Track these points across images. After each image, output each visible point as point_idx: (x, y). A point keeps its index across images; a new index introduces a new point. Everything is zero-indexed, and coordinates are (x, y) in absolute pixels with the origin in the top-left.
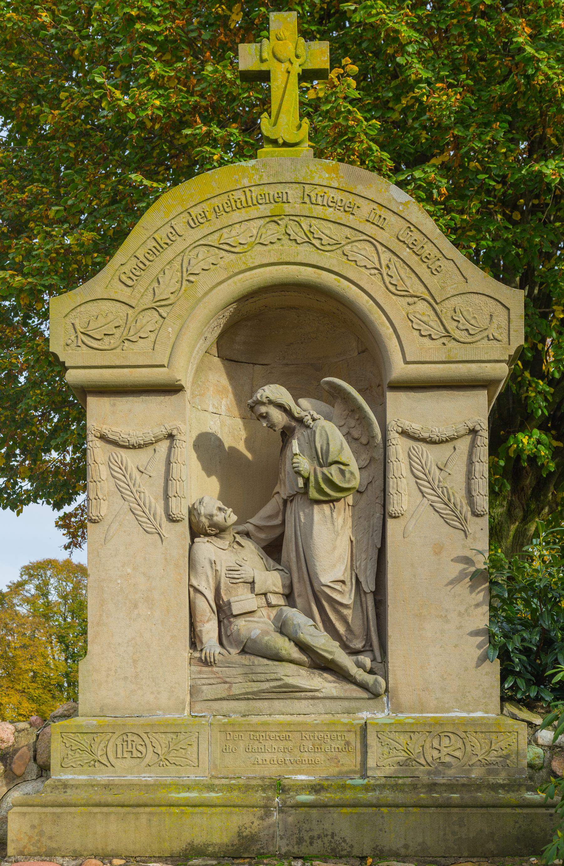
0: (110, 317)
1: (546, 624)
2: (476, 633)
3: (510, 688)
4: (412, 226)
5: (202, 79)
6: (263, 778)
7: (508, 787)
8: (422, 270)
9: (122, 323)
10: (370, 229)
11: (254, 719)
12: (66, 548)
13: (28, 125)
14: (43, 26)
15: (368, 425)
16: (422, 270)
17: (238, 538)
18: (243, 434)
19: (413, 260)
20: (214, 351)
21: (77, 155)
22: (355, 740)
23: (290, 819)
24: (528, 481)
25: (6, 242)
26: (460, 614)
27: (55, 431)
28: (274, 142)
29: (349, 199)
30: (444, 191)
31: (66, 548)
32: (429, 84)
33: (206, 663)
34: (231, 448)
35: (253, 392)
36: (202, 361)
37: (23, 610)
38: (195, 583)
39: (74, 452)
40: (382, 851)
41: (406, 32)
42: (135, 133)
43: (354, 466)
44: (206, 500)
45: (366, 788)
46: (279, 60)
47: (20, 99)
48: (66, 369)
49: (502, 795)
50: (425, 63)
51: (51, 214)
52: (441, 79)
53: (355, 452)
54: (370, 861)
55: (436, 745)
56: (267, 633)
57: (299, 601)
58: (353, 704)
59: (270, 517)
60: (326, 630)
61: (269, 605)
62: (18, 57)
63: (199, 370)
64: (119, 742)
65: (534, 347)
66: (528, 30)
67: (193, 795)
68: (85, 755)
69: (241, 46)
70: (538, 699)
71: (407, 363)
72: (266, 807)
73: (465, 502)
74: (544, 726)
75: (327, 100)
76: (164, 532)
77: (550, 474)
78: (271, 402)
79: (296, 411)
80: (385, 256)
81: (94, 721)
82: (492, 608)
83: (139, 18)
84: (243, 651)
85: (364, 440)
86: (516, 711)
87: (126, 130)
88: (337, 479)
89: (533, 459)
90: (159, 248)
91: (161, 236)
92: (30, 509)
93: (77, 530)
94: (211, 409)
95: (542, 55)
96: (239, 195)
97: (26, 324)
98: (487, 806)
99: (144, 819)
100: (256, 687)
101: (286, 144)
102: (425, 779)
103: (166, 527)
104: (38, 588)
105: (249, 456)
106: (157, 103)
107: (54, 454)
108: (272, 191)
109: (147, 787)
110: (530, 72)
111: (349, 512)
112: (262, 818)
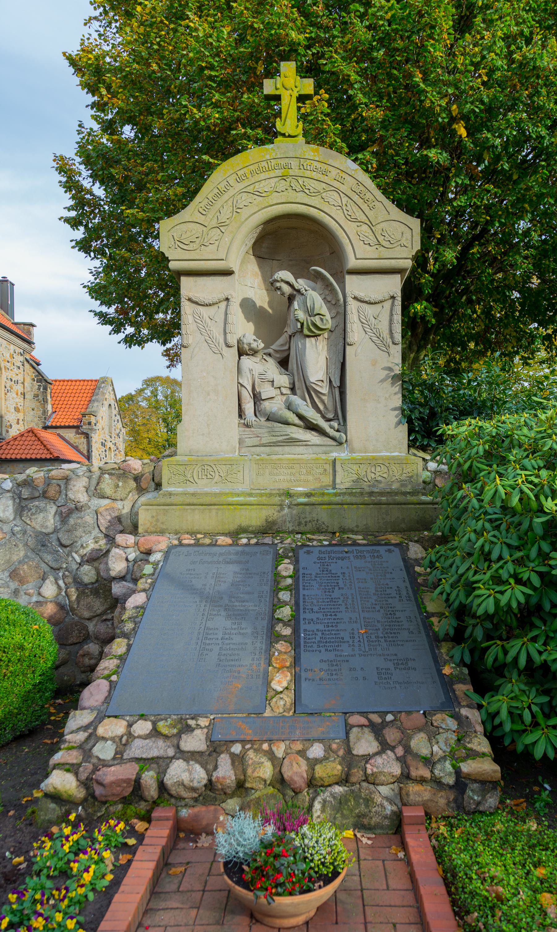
0: (194, 232)
1: (432, 404)
2: (395, 409)
3: (413, 440)
4: (359, 183)
5: (241, 103)
6: (279, 489)
7: (412, 494)
8: (365, 207)
9: (200, 235)
10: (337, 184)
11: (274, 457)
12: (168, 367)
13: (146, 129)
14: (154, 72)
15: (336, 294)
16: (365, 207)
17: (265, 357)
18: (267, 299)
19: (360, 202)
20: (251, 252)
21: (173, 146)
22: (329, 469)
23: (294, 512)
24: (420, 330)
25: (134, 195)
26: (386, 399)
27: (162, 302)
28: (283, 135)
29: (324, 167)
30: (375, 166)
31: (168, 367)
32: (366, 106)
33: (247, 426)
34: (260, 307)
35: (272, 276)
36: (244, 258)
37: (144, 404)
38: (241, 381)
39: (172, 314)
40: (344, 529)
41: (354, 77)
42: (205, 133)
43: (328, 317)
44: (247, 335)
45: (335, 495)
46: (286, 89)
47: (141, 114)
48: (169, 261)
49: (409, 498)
50: (364, 94)
51: (159, 177)
52: (373, 103)
53: (329, 309)
54: (338, 534)
55: (373, 471)
56: (281, 409)
57: (298, 392)
58: (328, 448)
59: (282, 345)
60: (313, 407)
61: (282, 394)
62: (141, 90)
63: (243, 262)
64: (200, 470)
65: (423, 255)
66: (420, 76)
67: (241, 499)
68: (181, 477)
69: (265, 81)
70: (428, 445)
71: (357, 259)
72: (281, 505)
73: (388, 336)
74: (431, 460)
75: (311, 114)
76: (223, 353)
77: (433, 325)
78: (282, 280)
79: (297, 286)
80: (345, 199)
81: (186, 458)
82: (403, 396)
83: (206, 68)
84: (268, 420)
85: (334, 302)
86: (415, 452)
87: (200, 131)
88: (319, 323)
89: (423, 318)
90: (220, 193)
91: (222, 186)
92: (149, 345)
93: (173, 357)
94: (249, 285)
95: (429, 89)
96: (264, 164)
97: (145, 242)
98: (401, 504)
99: (214, 512)
100: (275, 439)
101: (290, 136)
102: (367, 489)
103: (225, 350)
104: (152, 392)
105: (270, 311)
106: (217, 116)
107: (161, 315)
108: (283, 162)
109: (216, 495)
110: (423, 98)
111: (325, 342)
112: (279, 512)
